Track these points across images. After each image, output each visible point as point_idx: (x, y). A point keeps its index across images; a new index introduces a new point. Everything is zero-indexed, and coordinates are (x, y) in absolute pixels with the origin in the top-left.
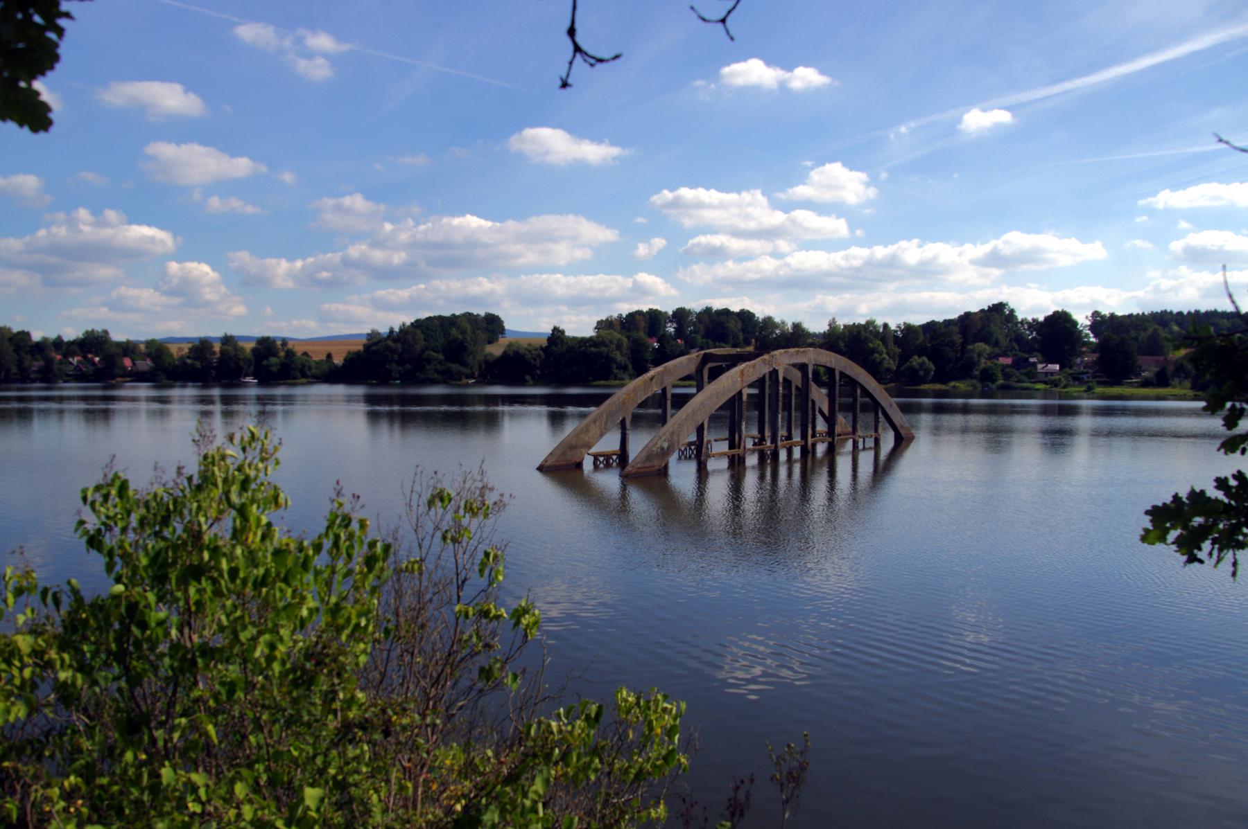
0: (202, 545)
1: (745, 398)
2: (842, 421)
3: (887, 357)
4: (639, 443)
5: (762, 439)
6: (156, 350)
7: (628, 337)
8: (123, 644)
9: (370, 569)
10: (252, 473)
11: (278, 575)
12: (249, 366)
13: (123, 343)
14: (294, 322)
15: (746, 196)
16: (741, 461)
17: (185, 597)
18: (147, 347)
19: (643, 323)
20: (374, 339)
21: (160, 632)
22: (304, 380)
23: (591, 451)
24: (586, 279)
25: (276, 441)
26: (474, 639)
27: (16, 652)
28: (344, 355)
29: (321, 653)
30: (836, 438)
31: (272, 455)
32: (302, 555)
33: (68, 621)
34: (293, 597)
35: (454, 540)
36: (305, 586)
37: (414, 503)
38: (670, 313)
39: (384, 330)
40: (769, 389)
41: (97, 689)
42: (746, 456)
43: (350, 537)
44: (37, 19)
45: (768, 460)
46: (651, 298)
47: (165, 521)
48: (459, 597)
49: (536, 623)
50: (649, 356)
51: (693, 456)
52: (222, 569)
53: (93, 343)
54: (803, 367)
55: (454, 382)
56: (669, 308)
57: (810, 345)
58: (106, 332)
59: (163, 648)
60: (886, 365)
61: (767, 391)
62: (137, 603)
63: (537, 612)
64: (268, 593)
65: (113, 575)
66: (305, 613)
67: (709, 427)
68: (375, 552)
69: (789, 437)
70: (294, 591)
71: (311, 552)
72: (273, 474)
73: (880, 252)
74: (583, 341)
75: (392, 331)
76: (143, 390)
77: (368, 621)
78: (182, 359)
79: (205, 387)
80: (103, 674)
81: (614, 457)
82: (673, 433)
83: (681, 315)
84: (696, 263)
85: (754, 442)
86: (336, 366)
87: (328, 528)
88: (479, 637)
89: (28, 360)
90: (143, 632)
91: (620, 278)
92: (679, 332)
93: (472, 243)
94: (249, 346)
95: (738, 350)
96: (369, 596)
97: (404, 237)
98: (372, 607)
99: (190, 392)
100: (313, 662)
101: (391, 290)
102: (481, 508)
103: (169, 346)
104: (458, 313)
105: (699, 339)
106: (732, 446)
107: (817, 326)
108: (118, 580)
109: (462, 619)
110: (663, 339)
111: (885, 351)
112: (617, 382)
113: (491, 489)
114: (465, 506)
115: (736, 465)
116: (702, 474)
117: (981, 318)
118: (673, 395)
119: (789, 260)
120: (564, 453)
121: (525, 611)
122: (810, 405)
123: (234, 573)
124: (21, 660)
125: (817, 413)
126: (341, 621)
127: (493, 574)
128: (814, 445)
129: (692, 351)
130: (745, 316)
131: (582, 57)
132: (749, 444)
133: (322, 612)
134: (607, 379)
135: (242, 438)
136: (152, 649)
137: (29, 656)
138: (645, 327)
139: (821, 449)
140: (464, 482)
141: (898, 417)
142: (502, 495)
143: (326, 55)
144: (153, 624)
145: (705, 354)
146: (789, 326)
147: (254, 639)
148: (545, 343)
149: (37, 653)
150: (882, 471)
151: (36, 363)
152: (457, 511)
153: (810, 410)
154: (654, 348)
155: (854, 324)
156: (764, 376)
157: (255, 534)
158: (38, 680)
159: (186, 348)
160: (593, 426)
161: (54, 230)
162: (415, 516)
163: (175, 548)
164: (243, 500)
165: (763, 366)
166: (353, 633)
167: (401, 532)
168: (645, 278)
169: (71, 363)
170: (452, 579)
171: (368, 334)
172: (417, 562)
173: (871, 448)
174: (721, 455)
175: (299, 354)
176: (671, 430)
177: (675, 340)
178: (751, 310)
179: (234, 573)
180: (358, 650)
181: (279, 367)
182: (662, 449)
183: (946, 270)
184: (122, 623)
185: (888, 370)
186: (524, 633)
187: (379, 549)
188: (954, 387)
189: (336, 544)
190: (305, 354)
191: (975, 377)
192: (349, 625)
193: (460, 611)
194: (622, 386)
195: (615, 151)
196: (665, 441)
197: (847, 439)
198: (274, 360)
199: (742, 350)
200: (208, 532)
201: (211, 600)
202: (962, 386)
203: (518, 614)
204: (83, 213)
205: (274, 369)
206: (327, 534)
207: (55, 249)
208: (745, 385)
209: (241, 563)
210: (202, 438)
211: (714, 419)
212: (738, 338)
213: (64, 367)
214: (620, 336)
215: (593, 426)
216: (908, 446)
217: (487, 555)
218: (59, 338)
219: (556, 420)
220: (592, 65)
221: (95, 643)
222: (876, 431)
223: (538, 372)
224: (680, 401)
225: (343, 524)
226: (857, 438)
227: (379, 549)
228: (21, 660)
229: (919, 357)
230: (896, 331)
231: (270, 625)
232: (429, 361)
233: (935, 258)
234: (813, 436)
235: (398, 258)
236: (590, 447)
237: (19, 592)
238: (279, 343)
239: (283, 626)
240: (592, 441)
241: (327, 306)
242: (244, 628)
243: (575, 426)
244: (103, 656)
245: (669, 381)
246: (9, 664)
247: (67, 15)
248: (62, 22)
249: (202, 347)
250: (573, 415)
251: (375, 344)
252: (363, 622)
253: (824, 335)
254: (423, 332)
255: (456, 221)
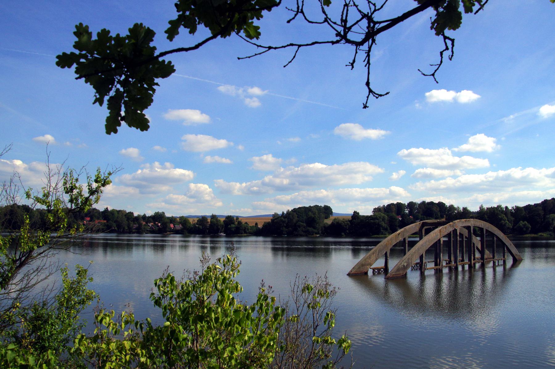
0: (204, 306)
1: (442, 242)
2: (487, 253)
3: (508, 222)
4: (393, 264)
5: (450, 261)
6: (184, 221)
7: (388, 215)
8: (168, 347)
9: (276, 320)
10: (228, 276)
11: (236, 321)
12: (222, 228)
13: (170, 217)
14: (242, 209)
15: (441, 150)
16: (441, 271)
17: (195, 328)
18: (180, 220)
19: (394, 209)
20: (275, 216)
21: (184, 343)
22: (245, 235)
23: (372, 267)
24: (369, 190)
25: (238, 262)
26: (321, 353)
27: (124, 348)
28: (263, 224)
29: (253, 357)
30: (485, 261)
31: (236, 268)
32: (247, 313)
33: (146, 336)
34: (241, 331)
35: (313, 308)
36: (247, 326)
37: (295, 290)
38: (406, 204)
39: (280, 213)
40: (453, 238)
41: (155, 366)
42: (443, 269)
43: (267, 305)
44: (145, 86)
45: (453, 271)
46: (398, 198)
47: (188, 295)
48: (314, 333)
49: (349, 346)
50: (397, 224)
51: (418, 269)
52: (212, 317)
53: (158, 217)
54: (468, 228)
55: (310, 236)
56: (406, 202)
57: (472, 217)
58: (164, 213)
59: (184, 350)
60: (507, 225)
61: (452, 239)
62: (175, 330)
63: (349, 341)
64: (231, 329)
65: (166, 318)
66: (246, 338)
67: (425, 255)
68: (278, 312)
69: (463, 260)
70: (242, 328)
71: (250, 311)
72: (236, 277)
73: (501, 173)
74: (367, 217)
75: (283, 213)
76: (178, 238)
77: (274, 343)
78: (194, 224)
79: (203, 237)
80: (158, 359)
81: (382, 270)
82: (409, 259)
83: (411, 205)
84: (418, 182)
85: (446, 262)
86: (259, 228)
87: (258, 301)
88: (323, 352)
89: (132, 224)
90: (177, 343)
91: (384, 189)
92: (411, 213)
93: (318, 174)
94: (222, 220)
95: (438, 220)
96: (274, 332)
97: (288, 173)
98: (276, 337)
99: (197, 239)
100: (250, 360)
101: (282, 196)
102: (325, 294)
103: (189, 219)
104: (312, 206)
105: (420, 216)
106: (436, 265)
107: (474, 208)
108: (168, 320)
109: (315, 343)
110: (403, 216)
111: (506, 219)
112: (383, 236)
113: (330, 285)
114: (318, 292)
115: (438, 273)
116: (423, 278)
117: (552, 202)
118: (409, 242)
119: (460, 178)
120: (359, 268)
121: (344, 341)
122: (472, 246)
123: (217, 319)
124: (126, 352)
125: (476, 249)
126: (262, 342)
127: (330, 323)
128: (474, 264)
129: (417, 221)
130: (441, 205)
131: (372, 94)
132: (444, 264)
133: (254, 338)
134: (378, 234)
135: (224, 260)
136: (180, 351)
137: (129, 350)
138: (395, 211)
139: (478, 265)
140: (318, 282)
141: (514, 250)
142: (334, 288)
143: (258, 97)
144: (181, 340)
145: (423, 222)
146: (461, 209)
147: (224, 349)
148: (350, 219)
149: (133, 349)
150: (506, 275)
151: (135, 225)
152: (314, 294)
153: (472, 247)
154: (399, 220)
155: (492, 207)
156: (450, 232)
157: (227, 303)
158: (132, 361)
159: (196, 220)
160: (372, 255)
161: (145, 170)
162: (295, 296)
163: (192, 307)
164: (223, 288)
165: (450, 228)
166: (267, 347)
167: (290, 302)
168: (394, 189)
169: (149, 226)
170: (312, 325)
171: (273, 215)
172: (296, 317)
173: (501, 265)
174: (431, 269)
175: (243, 223)
176: (408, 257)
177: (409, 216)
178: (444, 202)
179: (217, 319)
180: (269, 355)
181: (235, 229)
182: (404, 266)
183: (536, 181)
184: (168, 338)
185: (508, 228)
186: (343, 351)
187: (280, 311)
188: (541, 235)
189: (261, 308)
190: (246, 223)
191: (551, 231)
192: (265, 345)
193: (315, 340)
194: (386, 237)
195: (383, 132)
196: (405, 262)
197: (490, 261)
198: (233, 226)
199: (440, 220)
200: (207, 301)
201: (207, 330)
202: (545, 235)
203: (341, 342)
204: (157, 164)
205: (233, 229)
206: (257, 304)
207: (145, 179)
208: (442, 236)
209: (220, 315)
210: (204, 260)
211: (428, 251)
212: (438, 215)
213: (146, 227)
214: (384, 215)
215: (372, 255)
216: (520, 263)
217: (328, 315)
218: (145, 215)
219: (356, 252)
220: (377, 98)
221: (155, 346)
222: (504, 257)
223: (348, 231)
224: (412, 244)
225: (264, 299)
226: (495, 260)
227: (280, 311)
228: (126, 352)
229: (523, 222)
230: (512, 210)
231: (231, 343)
232: (299, 226)
233: (528, 175)
234: (474, 259)
235: (286, 182)
236: (371, 265)
237: (127, 322)
238: (235, 218)
239: (237, 344)
240: (372, 262)
241: (256, 203)
242: (220, 344)
243: (364, 255)
244: (160, 352)
245: (407, 235)
246: (121, 353)
247: (157, 84)
248: (155, 87)
249: (203, 220)
250: (363, 249)
251: (276, 219)
252: (272, 344)
253: (478, 213)
254: (297, 214)
255: (311, 166)
